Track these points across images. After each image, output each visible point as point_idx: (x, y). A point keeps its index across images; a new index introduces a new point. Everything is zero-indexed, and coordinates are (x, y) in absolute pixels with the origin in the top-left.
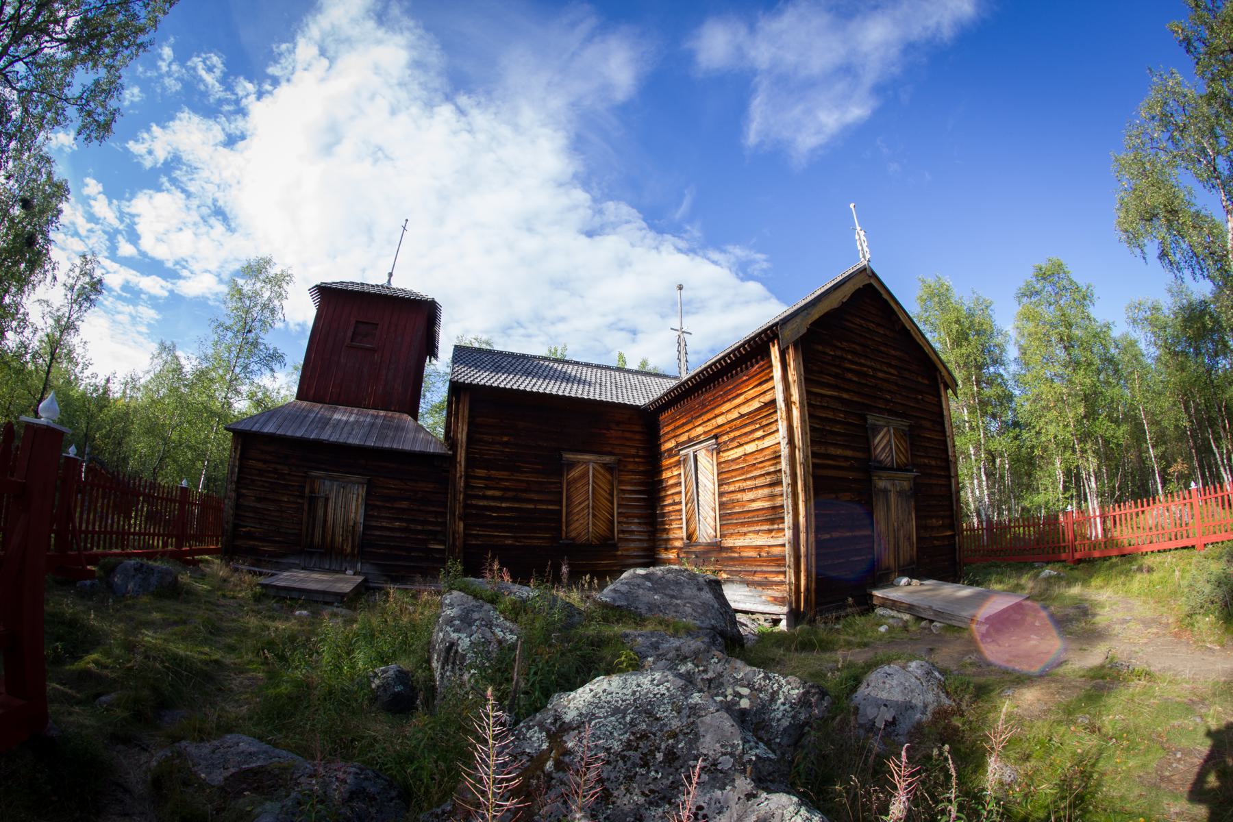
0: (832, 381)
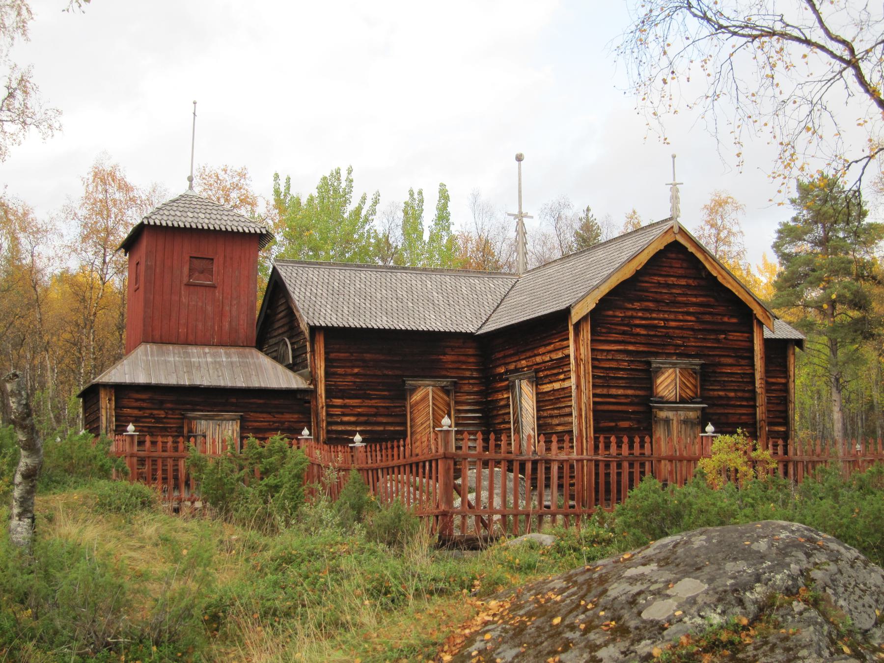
0: (620, 337)
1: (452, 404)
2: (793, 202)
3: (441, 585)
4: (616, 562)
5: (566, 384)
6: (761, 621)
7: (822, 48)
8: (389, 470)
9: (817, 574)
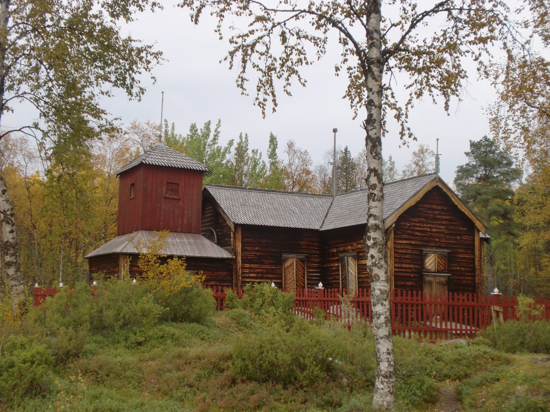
0: (407, 236)
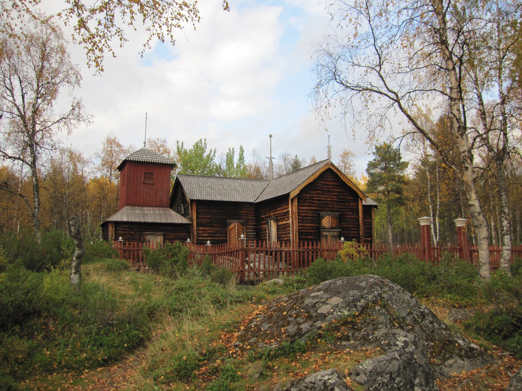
0: (308, 204)
1: (245, 229)
2: (374, 153)
3: (240, 299)
4: (308, 290)
5: (288, 222)
6: (363, 313)
7: (386, 95)
8: (220, 254)
9: (384, 295)
